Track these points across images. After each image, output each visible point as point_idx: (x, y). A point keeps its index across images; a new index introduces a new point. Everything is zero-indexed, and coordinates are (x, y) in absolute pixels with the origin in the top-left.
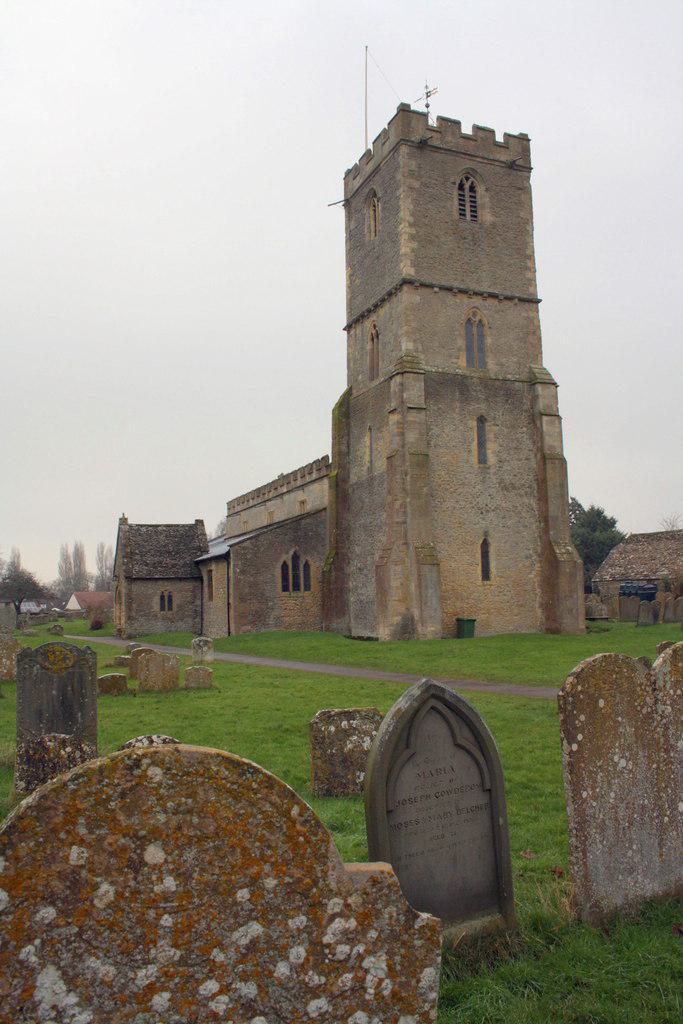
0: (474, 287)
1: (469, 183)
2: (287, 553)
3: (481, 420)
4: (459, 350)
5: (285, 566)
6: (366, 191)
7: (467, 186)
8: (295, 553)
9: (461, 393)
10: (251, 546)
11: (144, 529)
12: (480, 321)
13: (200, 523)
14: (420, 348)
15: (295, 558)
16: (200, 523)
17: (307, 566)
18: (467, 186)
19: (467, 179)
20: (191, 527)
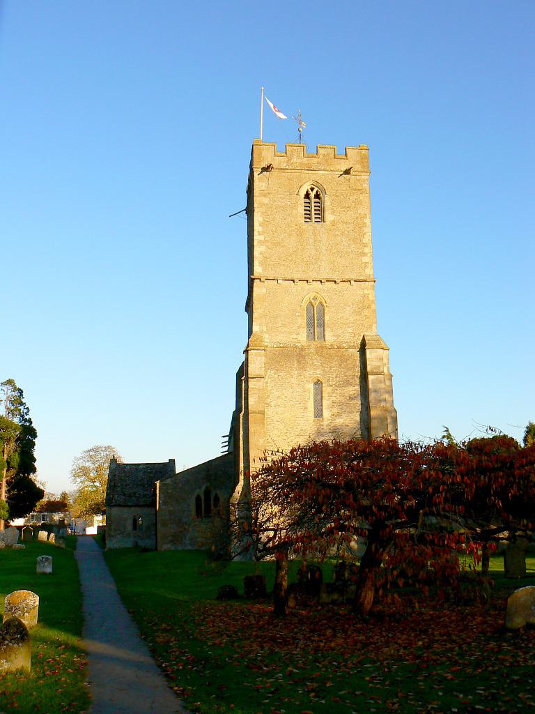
0: (312, 275)
1: (315, 192)
2: (200, 488)
3: (318, 383)
4: (299, 327)
5: (198, 498)
6: (35, 469)
7: (312, 194)
8: (207, 487)
9: (299, 362)
10: (170, 482)
11: (193, 470)
12: (321, 303)
13: (172, 461)
14: (265, 329)
15: (207, 492)
16: (172, 461)
17: (217, 498)
18: (312, 194)
19: (312, 189)
20: (164, 464)
